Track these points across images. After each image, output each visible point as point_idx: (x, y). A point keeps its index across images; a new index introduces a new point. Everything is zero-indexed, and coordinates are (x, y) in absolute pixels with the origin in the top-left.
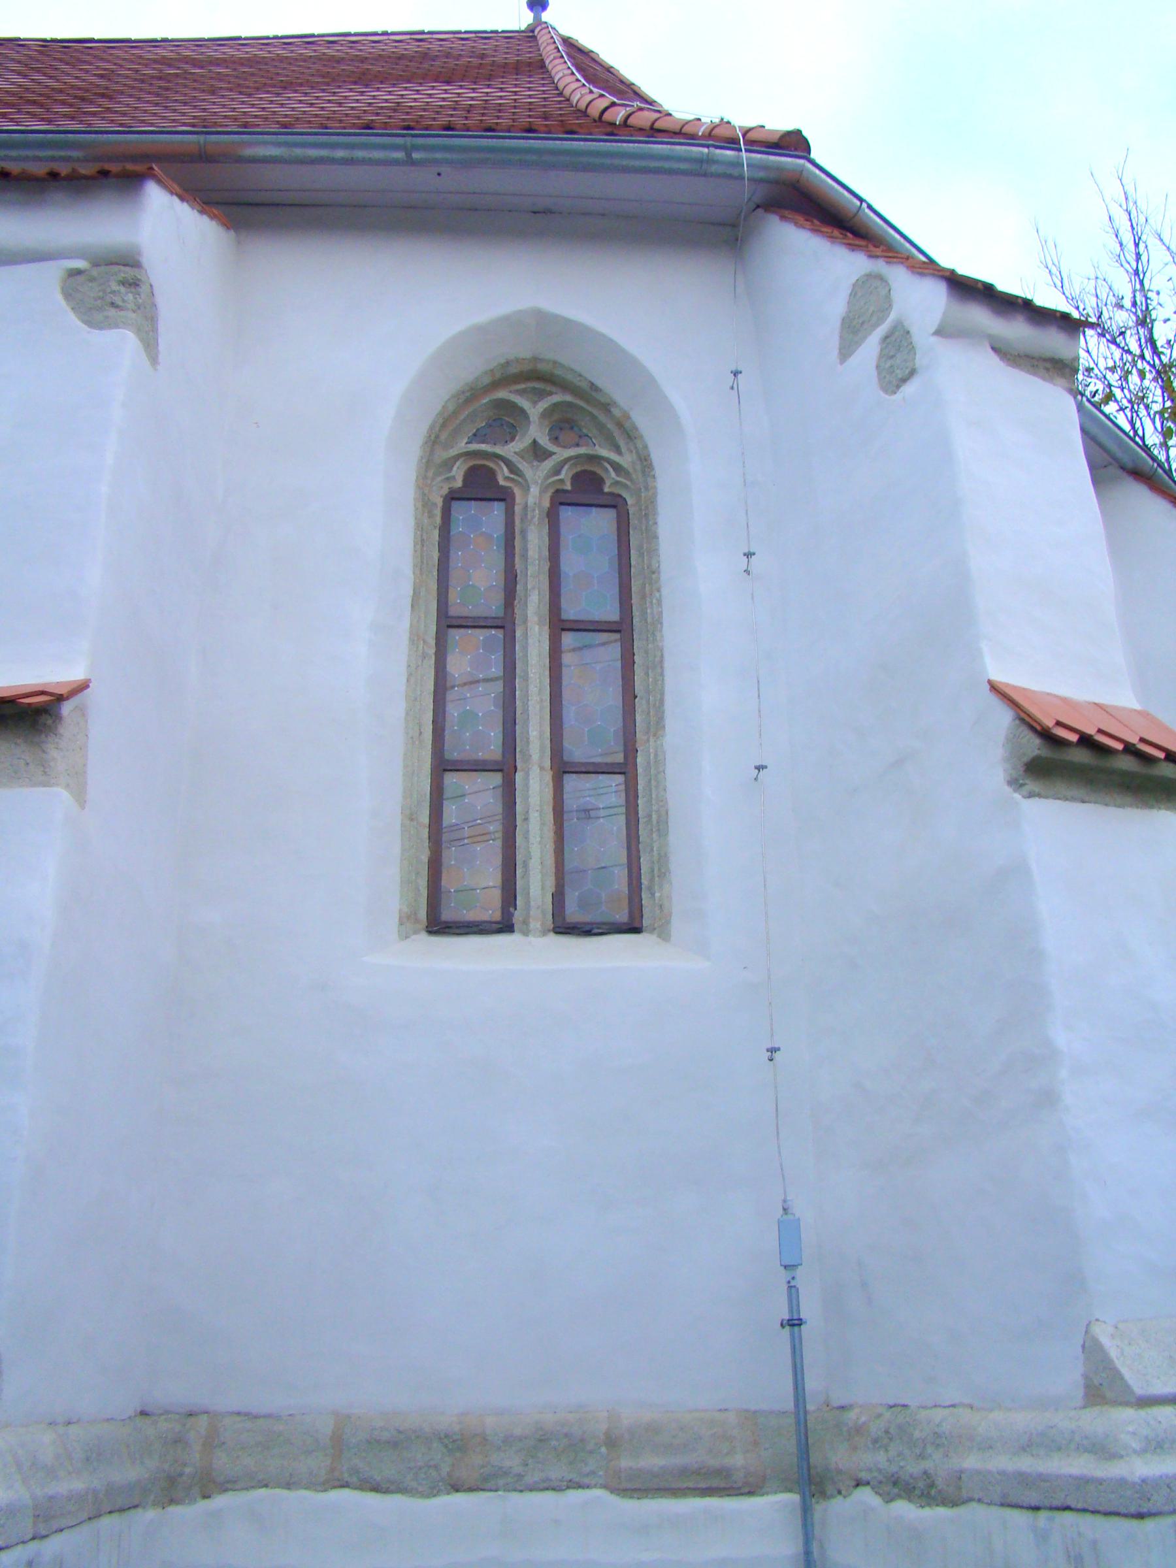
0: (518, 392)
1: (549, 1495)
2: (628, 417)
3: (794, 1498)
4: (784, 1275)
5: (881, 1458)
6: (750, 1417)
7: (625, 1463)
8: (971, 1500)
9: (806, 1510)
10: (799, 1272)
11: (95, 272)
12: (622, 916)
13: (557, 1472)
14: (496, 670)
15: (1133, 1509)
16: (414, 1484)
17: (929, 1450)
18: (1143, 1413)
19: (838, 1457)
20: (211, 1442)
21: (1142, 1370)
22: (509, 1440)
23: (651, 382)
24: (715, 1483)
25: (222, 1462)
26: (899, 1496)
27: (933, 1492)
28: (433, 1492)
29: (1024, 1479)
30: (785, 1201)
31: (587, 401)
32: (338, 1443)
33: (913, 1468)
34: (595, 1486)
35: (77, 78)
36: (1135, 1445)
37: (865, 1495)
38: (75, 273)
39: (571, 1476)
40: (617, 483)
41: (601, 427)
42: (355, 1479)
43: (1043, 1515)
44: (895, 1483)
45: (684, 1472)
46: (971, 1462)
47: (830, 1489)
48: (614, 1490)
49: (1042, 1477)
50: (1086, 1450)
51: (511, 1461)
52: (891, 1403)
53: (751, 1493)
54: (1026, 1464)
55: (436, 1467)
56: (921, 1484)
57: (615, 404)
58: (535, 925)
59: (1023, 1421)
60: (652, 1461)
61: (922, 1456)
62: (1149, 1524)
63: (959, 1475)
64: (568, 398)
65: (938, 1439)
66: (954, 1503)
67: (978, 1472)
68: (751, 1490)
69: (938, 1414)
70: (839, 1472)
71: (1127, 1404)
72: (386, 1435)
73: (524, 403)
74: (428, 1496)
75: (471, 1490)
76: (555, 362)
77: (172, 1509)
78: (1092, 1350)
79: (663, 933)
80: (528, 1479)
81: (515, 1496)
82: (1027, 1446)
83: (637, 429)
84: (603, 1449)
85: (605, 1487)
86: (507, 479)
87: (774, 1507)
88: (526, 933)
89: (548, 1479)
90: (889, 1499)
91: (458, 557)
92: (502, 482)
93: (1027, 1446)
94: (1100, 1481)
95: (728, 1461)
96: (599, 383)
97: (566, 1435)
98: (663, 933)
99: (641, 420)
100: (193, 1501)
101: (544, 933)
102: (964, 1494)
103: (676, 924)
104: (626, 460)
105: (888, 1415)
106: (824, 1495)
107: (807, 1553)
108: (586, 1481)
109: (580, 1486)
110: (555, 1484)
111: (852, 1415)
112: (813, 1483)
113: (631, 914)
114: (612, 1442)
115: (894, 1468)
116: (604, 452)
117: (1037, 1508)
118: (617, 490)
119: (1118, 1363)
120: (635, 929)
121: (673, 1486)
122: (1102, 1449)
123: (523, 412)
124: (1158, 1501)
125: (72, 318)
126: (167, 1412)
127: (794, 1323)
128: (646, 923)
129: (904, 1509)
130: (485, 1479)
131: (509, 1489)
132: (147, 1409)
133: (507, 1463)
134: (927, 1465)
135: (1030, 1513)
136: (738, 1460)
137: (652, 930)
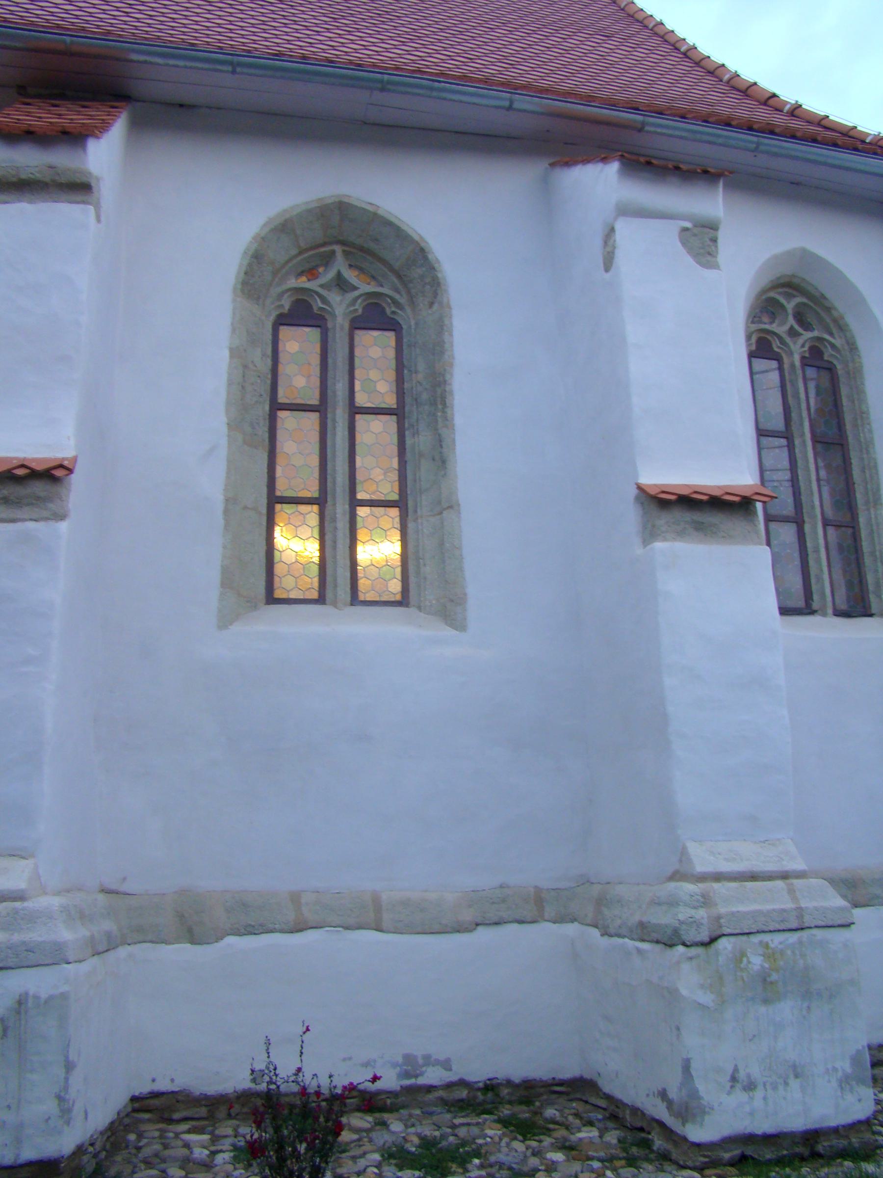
0: (780, 294)
2: (842, 318)
11: (696, 231)
14: (786, 464)
23: (862, 301)
31: (815, 304)
35: (776, 155)
38: (685, 230)
40: (832, 355)
41: (821, 320)
57: (835, 309)
64: (804, 300)
73: (783, 301)
75: (864, 906)
76: (804, 279)
83: (848, 325)
86: (779, 347)
91: (756, 393)
92: (776, 349)
96: (828, 296)
99: (850, 320)
104: (838, 342)
116: (827, 337)
118: (830, 359)
123: (782, 307)
125: (689, 260)
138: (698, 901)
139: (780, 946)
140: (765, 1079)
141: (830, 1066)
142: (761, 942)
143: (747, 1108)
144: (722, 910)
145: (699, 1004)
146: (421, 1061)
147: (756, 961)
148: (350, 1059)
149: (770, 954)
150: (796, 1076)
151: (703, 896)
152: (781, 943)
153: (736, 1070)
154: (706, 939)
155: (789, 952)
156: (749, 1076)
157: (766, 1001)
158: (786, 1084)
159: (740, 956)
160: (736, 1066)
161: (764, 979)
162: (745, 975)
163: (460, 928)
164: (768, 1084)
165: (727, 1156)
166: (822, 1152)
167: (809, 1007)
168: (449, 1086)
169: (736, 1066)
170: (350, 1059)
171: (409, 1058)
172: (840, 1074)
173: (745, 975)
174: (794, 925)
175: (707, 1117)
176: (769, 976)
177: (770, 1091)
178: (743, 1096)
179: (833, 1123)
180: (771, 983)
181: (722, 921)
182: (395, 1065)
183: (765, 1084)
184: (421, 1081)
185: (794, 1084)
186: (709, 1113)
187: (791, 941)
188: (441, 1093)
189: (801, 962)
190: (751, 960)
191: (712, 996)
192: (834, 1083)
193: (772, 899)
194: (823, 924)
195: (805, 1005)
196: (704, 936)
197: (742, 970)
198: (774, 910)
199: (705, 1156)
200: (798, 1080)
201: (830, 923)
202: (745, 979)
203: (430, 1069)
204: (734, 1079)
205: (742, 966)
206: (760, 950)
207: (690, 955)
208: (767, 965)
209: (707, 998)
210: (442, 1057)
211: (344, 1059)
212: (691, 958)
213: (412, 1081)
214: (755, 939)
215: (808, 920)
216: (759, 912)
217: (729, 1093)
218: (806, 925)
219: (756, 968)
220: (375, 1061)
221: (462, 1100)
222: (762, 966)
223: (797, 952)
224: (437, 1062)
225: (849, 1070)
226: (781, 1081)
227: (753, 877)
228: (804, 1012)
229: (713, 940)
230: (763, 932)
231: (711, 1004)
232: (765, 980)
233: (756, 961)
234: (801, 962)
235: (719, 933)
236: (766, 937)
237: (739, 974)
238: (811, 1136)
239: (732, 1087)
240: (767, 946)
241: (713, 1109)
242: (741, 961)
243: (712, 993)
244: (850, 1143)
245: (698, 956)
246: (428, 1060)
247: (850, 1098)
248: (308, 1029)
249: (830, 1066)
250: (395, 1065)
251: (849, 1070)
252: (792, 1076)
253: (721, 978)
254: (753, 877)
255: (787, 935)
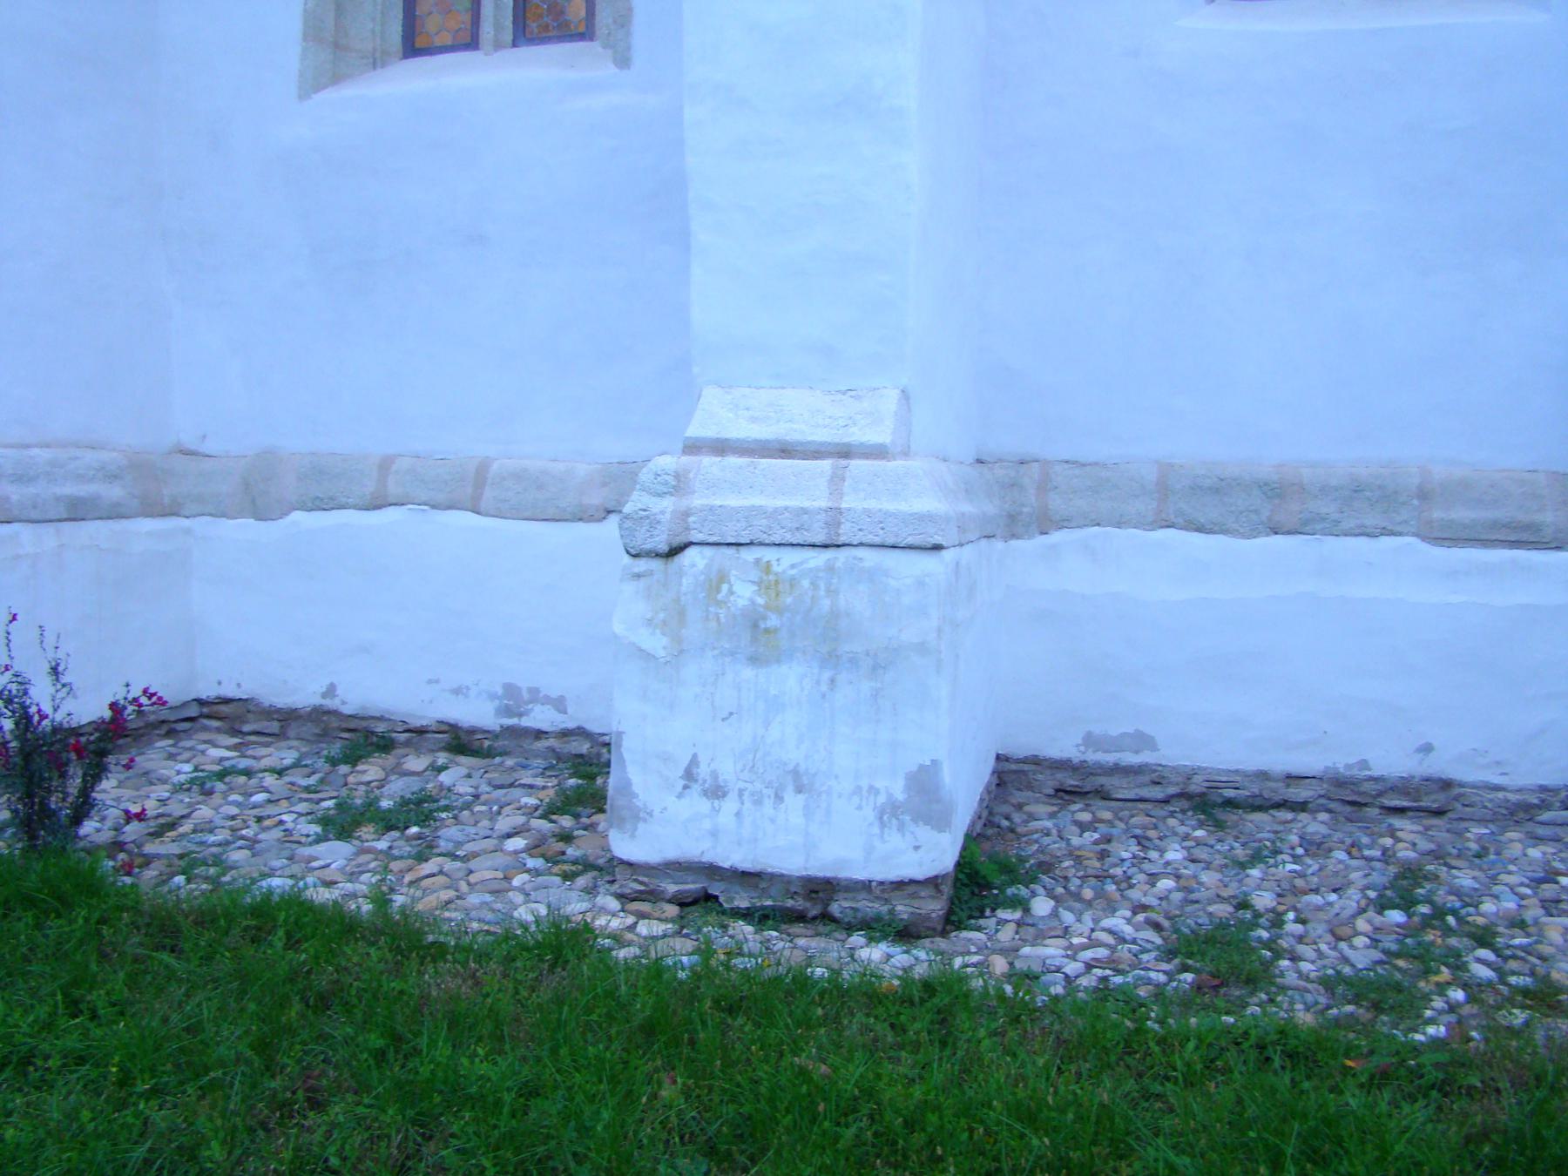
1: (1362, 540)
13: (1372, 520)
16: (1235, 526)
20: (1044, 486)
22: (1325, 490)
24: (1525, 536)
25: (1056, 503)
28: (1253, 533)
32: (1163, 489)
34: (1407, 534)
42: (1180, 520)
45: (1495, 525)
48: (1424, 539)
51: (1327, 508)
53: (1558, 548)
55: (1256, 512)
58: (487, 30)
60: (1461, 514)
72: (1208, 483)
75: (1289, 533)
77: (1014, 542)
80: (1345, 525)
81: (1331, 541)
84: (1415, 502)
89: (1363, 526)
95: (1538, 518)
97: (1380, 487)
100: (1031, 537)
108: (1399, 529)
114: (1424, 495)
126: (1001, 460)
130: (1306, 522)
132: (984, 458)
133: (1324, 510)
136: (1548, 517)
138: (666, 483)
139: (793, 572)
140: (741, 785)
141: (864, 783)
142: (758, 561)
143: (707, 824)
144: (697, 502)
145: (640, 650)
146: (526, 696)
147: (743, 593)
148: (437, 681)
149: (769, 582)
150: (799, 790)
151: (677, 476)
152: (793, 566)
153: (694, 761)
154: (664, 548)
155: (806, 583)
156: (714, 775)
157: (754, 660)
158: (779, 798)
159: (716, 582)
160: (695, 756)
161: (754, 622)
162: (722, 612)
163: (579, 517)
164: (746, 794)
165: (672, 888)
166: (837, 915)
167: (832, 681)
168: (565, 734)
169: (695, 756)
170: (437, 681)
171: (510, 690)
172: (882, 799)
173: (722, 612)
174: (820, 538)
175: (641, 826)
176: (764, 618)
177: (748, 805)
178: (704, 805)
179: (860, 875)
180: (767, 631)
181: (691, 519)
182: (493, 697)
183: (741, 792)
184: (526, 722)
185: (794, 802)
186: (645, 820)
187: (812, 564)
188: (552, 742)
189: (826, 603)
190: (735, 588)
191: (665, 641)
192: (869, 813)
193: (801, 490)
194: (877, 540)
195: (827, 675)
196: (661, 542)
197: (719, 603)
198: (786, 508)
199: (641, 883)
200: (801, 797)
201: (890, 541)
202: (723, 620)
203: (538, 708)
204: (689, 775)
205: (719, 597)
206: (754, 575)
207: (636, 570)
208: (760, 601)
209: (656, 643)
210: (554, 694)
211: (430, 682)
212: (638, 576)
213: (513, 721)
214: (749, 555)
215: (846, 533)
216: (760, 511)
217: (680, 796)
218: (842, 539)
219: (742, 603)
220: (468, 688)
221: (581, 756)
222: (753, 602)
223: (822, 585)
224: (547, 700)
225: (900, 796)
226: (771, 792)
227: (785, 450)
228: (824, 688)
229: (674, 551)
230: (762, 544)
231: (662, 653)
232: (755, 626)
233: (743, 593)
234: (826, 603)
235: (682, 539)
236: (769, 554)
237: (712, 609)
238: (821, 889)
239: (686, 787)
240: (768, 568)
241: (650, 814)
242: (718, 590)
243: (664, 634)
244: (892, 912)
245: (650, 573)
246: (535, 696)
247: (895, 840)
248: (14, 618)
249: (864, 783)
250: (493, 697)
251: (900, 796)
252: (790, 788)
253: (682, 614)
254: (785, 450)
255: (810, 553)
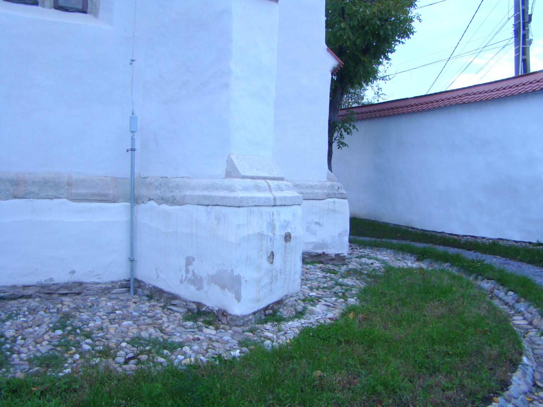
1: (48, 201)
3: (129, 204)
4: (130, 135)
5: (158, 192)
6: (115, 179)
7: (74, 191)
8: (187, 203)
9: (132, 207)
10: (136, 134)
12: (80, 7)
13: (51, 193)
15: (237, 205)
17: (174, 190)
18: (242, 180)
19: (143, 192)
21: (243, 169)
24: (103, 198)
26: (163, 203)
27: (175, 202)
28: (7, 199)
29: (205, 197)
30: (133, 111)
33: (169, 195)
36: (240, 188)
37: (152, 203)
39: (56, 195)
43: (210, 207)
44: (162, 199)
45: (93, 195)
46: (188, 193)
47: (140, 201)
49: (211, 197)
50: (225, 189)
51: (35, 189)
52: (162, 176)
53: (114, 202)
54: (206, 193)
55: (8, 190)
56: (171, 199)
59: (205, 181)
60: (83, 191)
61: (172, 191)
62: (241, 209)
63: (184, 197)
65: (178, 187)
66: (181, 205)
67: (191, 195)
68: (114, 200)
69: (178, 179)
70: (144, 196)
71: (238, 177)
74: (5, 200)
75: (20, 198)
78: (230, 162)
79: (95, 14)
80: (41, 195)
82: (207, 188)
85: (67, 198)
87: (121, 207)
88: (43, 6)
90: (160, 204)
93: (207, 188)
94: (229, 198)
97: (54, 182)
98: (95, 14)
101: (50, 8)
102: (186, 202)
103: (101, 12)
105: (161, 180)
106: (138, 203)
107: (132, 220)
108: (61, 196)
109: (58, 198)
110: (50, 197)
111: (149, 180)
112: (135, 200)
113: (83, 7)
114: (69, 184)
115: (162, 195)
117: (208, 205)
119: (237, 166)
120: (85, 12)
121: (90, 199)
122: (230, 189)
124: (244, 204)
127: (133, 150)
128: (88, 10)
129: (165, 207)
131: (33, 198)
134: (174, 194)
135: (206, 207)
136: (111, 192)
137: (91, 13)
